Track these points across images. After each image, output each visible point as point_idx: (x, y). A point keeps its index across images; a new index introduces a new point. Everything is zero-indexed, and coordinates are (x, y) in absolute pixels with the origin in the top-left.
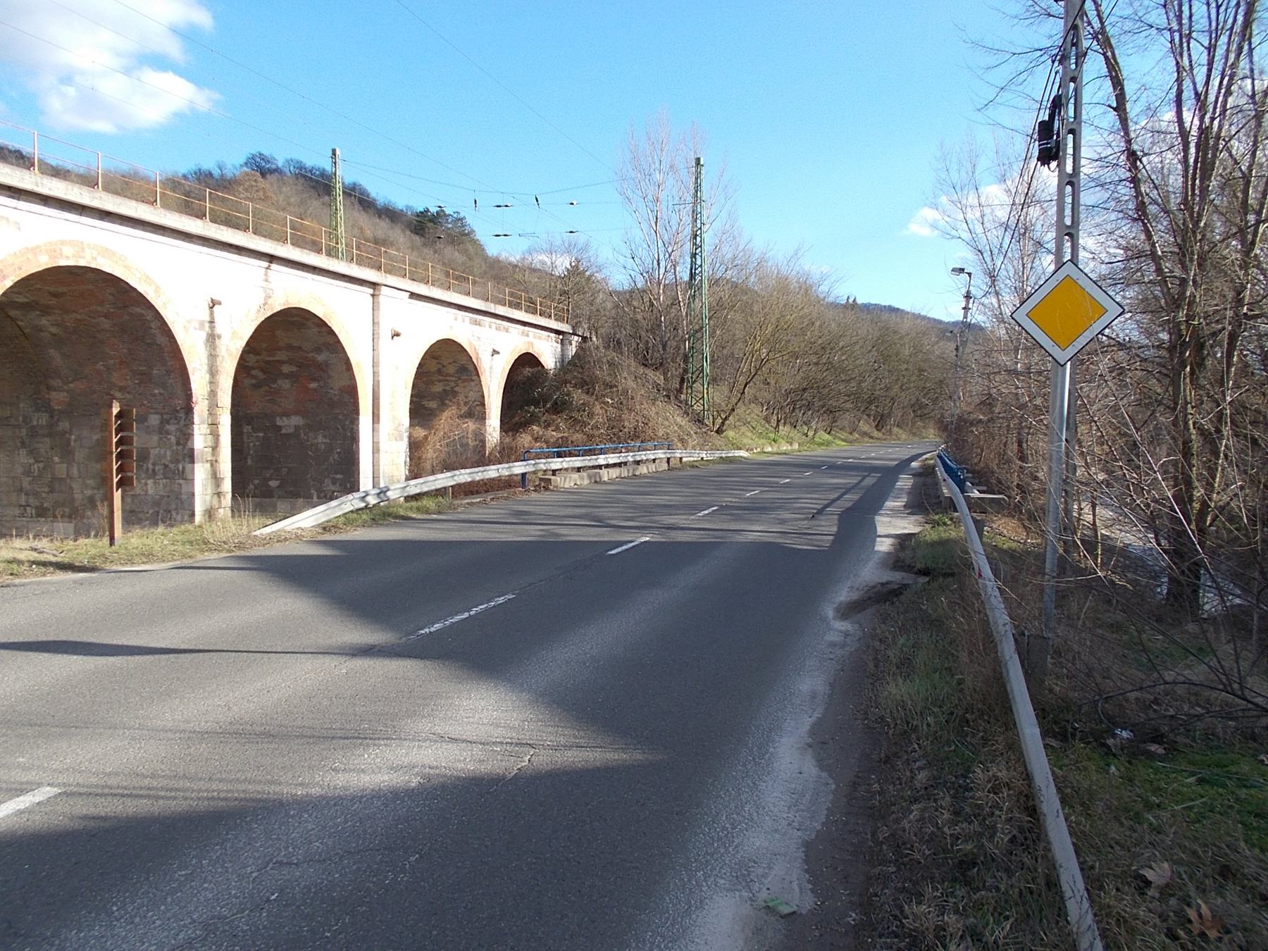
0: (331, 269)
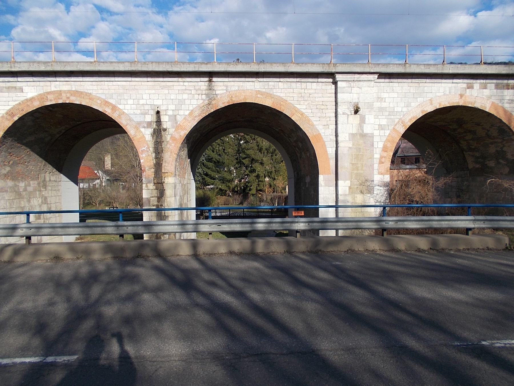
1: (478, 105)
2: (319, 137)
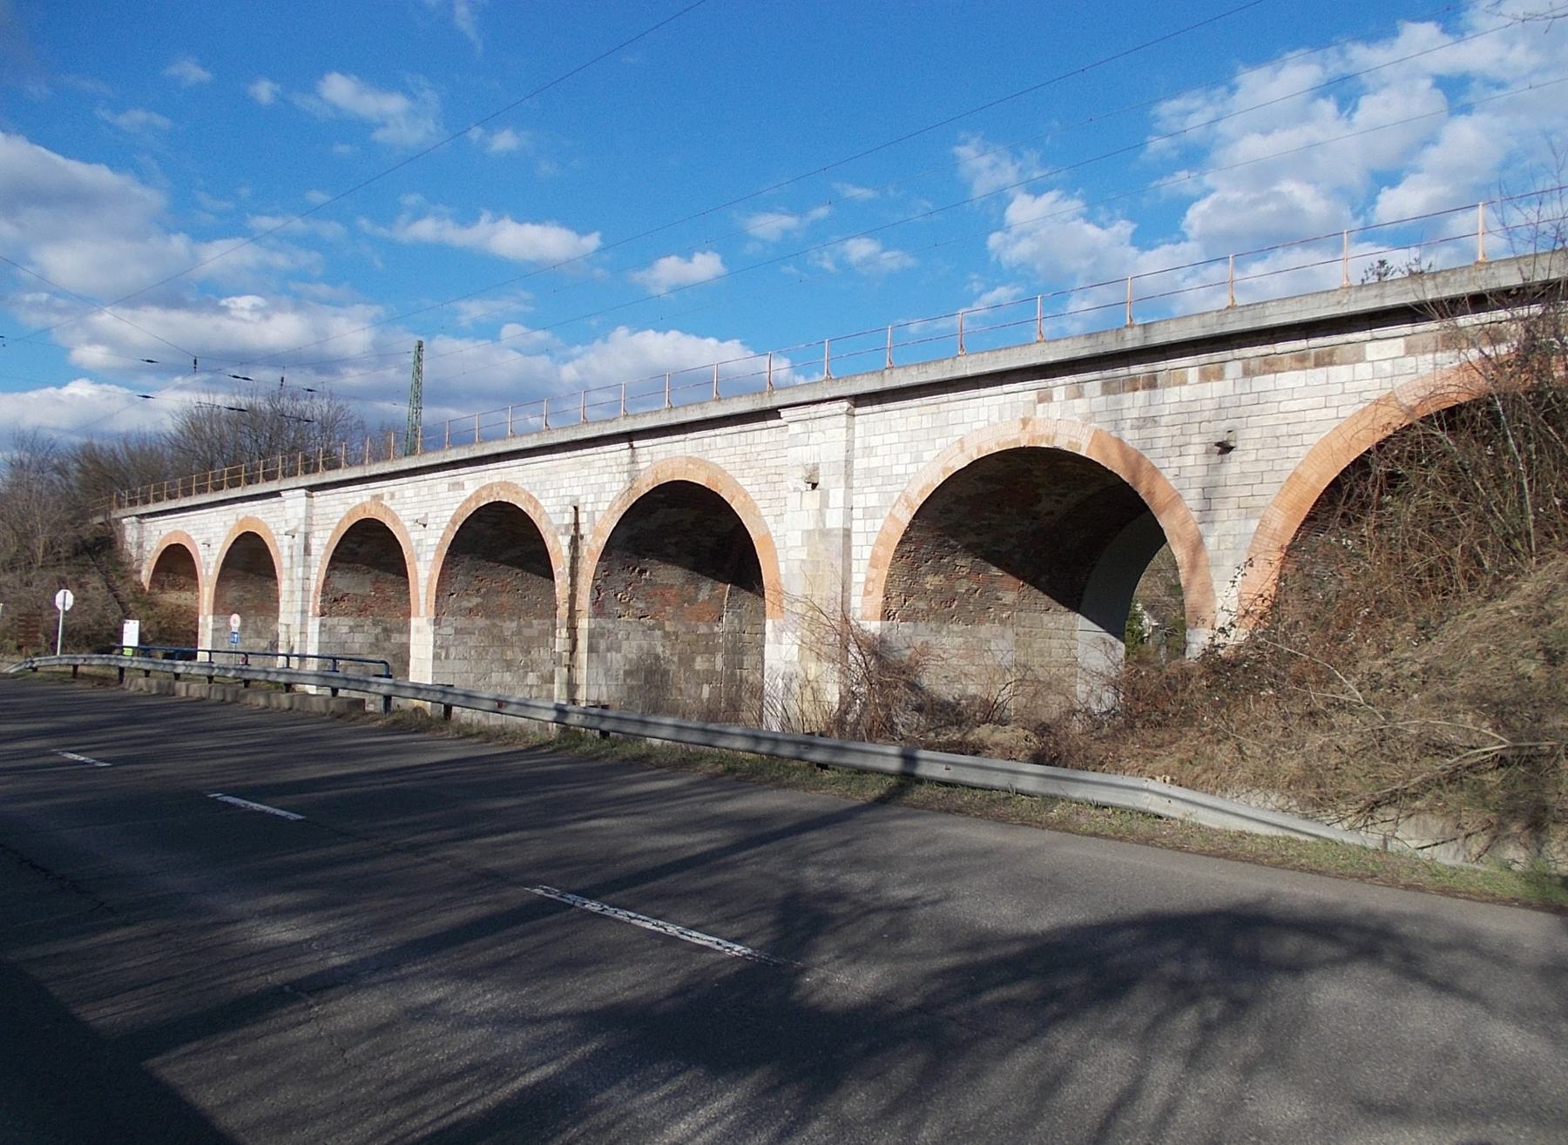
0: (674, 421)
1: (1062, 443)
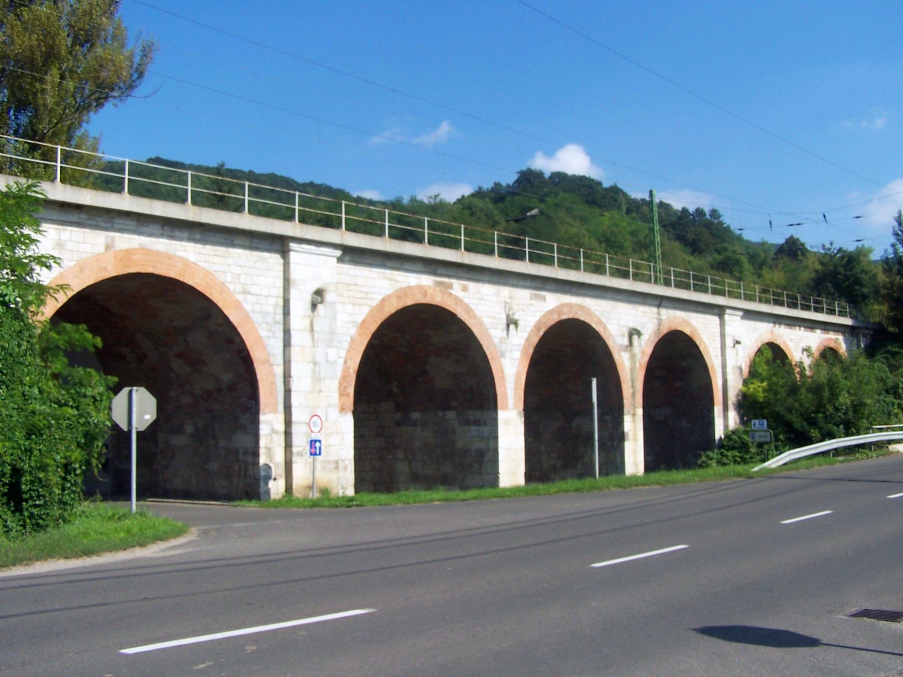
2: (713, 367)
